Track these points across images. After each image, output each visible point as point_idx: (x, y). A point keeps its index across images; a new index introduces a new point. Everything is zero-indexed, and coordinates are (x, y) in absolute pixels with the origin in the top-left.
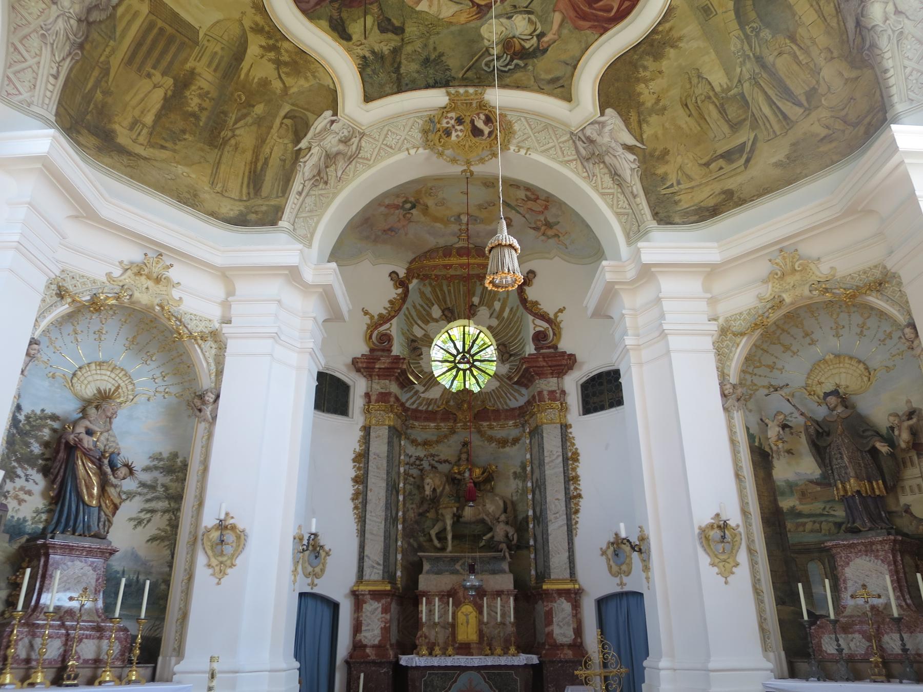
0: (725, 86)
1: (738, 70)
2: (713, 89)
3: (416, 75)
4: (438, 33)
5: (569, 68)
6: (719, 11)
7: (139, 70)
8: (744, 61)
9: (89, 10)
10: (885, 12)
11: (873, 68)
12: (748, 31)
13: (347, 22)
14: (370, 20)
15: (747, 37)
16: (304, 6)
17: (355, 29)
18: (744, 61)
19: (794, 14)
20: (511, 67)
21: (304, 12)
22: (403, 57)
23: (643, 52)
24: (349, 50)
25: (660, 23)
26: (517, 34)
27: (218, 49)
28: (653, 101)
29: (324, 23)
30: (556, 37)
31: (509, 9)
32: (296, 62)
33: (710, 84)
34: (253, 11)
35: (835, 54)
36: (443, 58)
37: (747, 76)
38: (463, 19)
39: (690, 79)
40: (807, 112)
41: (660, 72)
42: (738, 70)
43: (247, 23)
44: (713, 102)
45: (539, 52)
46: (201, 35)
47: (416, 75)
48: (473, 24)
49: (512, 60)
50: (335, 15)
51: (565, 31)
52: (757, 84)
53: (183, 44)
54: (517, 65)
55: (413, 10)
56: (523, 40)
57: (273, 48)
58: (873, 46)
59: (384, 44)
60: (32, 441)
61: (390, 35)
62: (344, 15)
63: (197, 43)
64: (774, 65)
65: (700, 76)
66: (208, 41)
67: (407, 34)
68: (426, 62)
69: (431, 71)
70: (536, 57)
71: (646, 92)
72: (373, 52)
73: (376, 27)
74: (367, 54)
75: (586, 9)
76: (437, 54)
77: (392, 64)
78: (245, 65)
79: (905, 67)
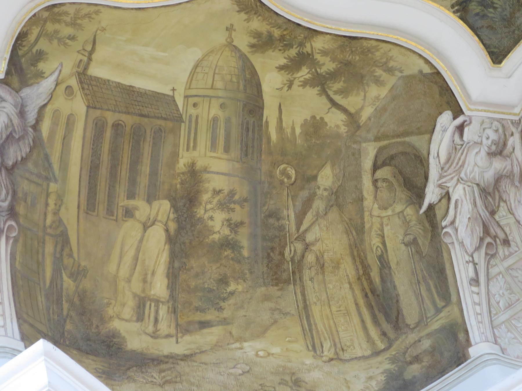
7: (110, 212)
27: (215, 111)
32: (348, 64)
34: (243, 16)
43: (243, 42)
46: (180, 102)
53: (159, 133)
63: (179, 119)
66: (195, 105)
78: (270, 113)
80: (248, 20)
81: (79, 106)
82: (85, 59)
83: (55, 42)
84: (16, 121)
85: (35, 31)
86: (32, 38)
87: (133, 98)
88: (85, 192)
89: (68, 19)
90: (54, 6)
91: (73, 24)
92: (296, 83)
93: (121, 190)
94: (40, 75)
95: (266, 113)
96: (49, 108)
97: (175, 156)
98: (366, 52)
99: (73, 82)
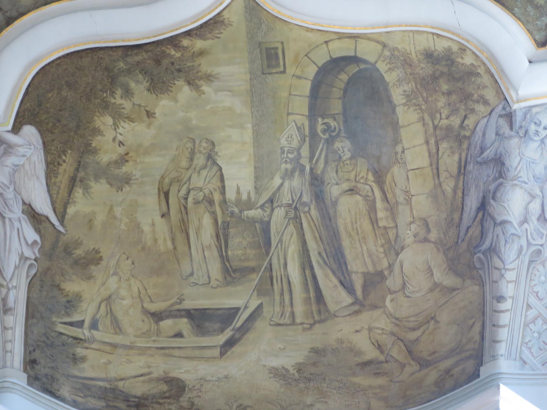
0: (244, 197)
1: (277, 181)
2: (223, 193)
6: (291, 70)
8: (293, 171)
10: (526, 208)
11: (482, 285)
12: (320, 128)
15: (313, 135)
18: (293, 171)
19: (397, 141)
23: (138, 63)
25: (188, 33)
28: (114, 157)
35: (433, 236)
37: (286, 199)
39: (193, 153)
41: (150, 114)
42: (277, 181)
52: (297, 221)
58: (493, 250)
64: (335, 203)
65: (211, 158)
71: (109, 134)
79: (529, 307)
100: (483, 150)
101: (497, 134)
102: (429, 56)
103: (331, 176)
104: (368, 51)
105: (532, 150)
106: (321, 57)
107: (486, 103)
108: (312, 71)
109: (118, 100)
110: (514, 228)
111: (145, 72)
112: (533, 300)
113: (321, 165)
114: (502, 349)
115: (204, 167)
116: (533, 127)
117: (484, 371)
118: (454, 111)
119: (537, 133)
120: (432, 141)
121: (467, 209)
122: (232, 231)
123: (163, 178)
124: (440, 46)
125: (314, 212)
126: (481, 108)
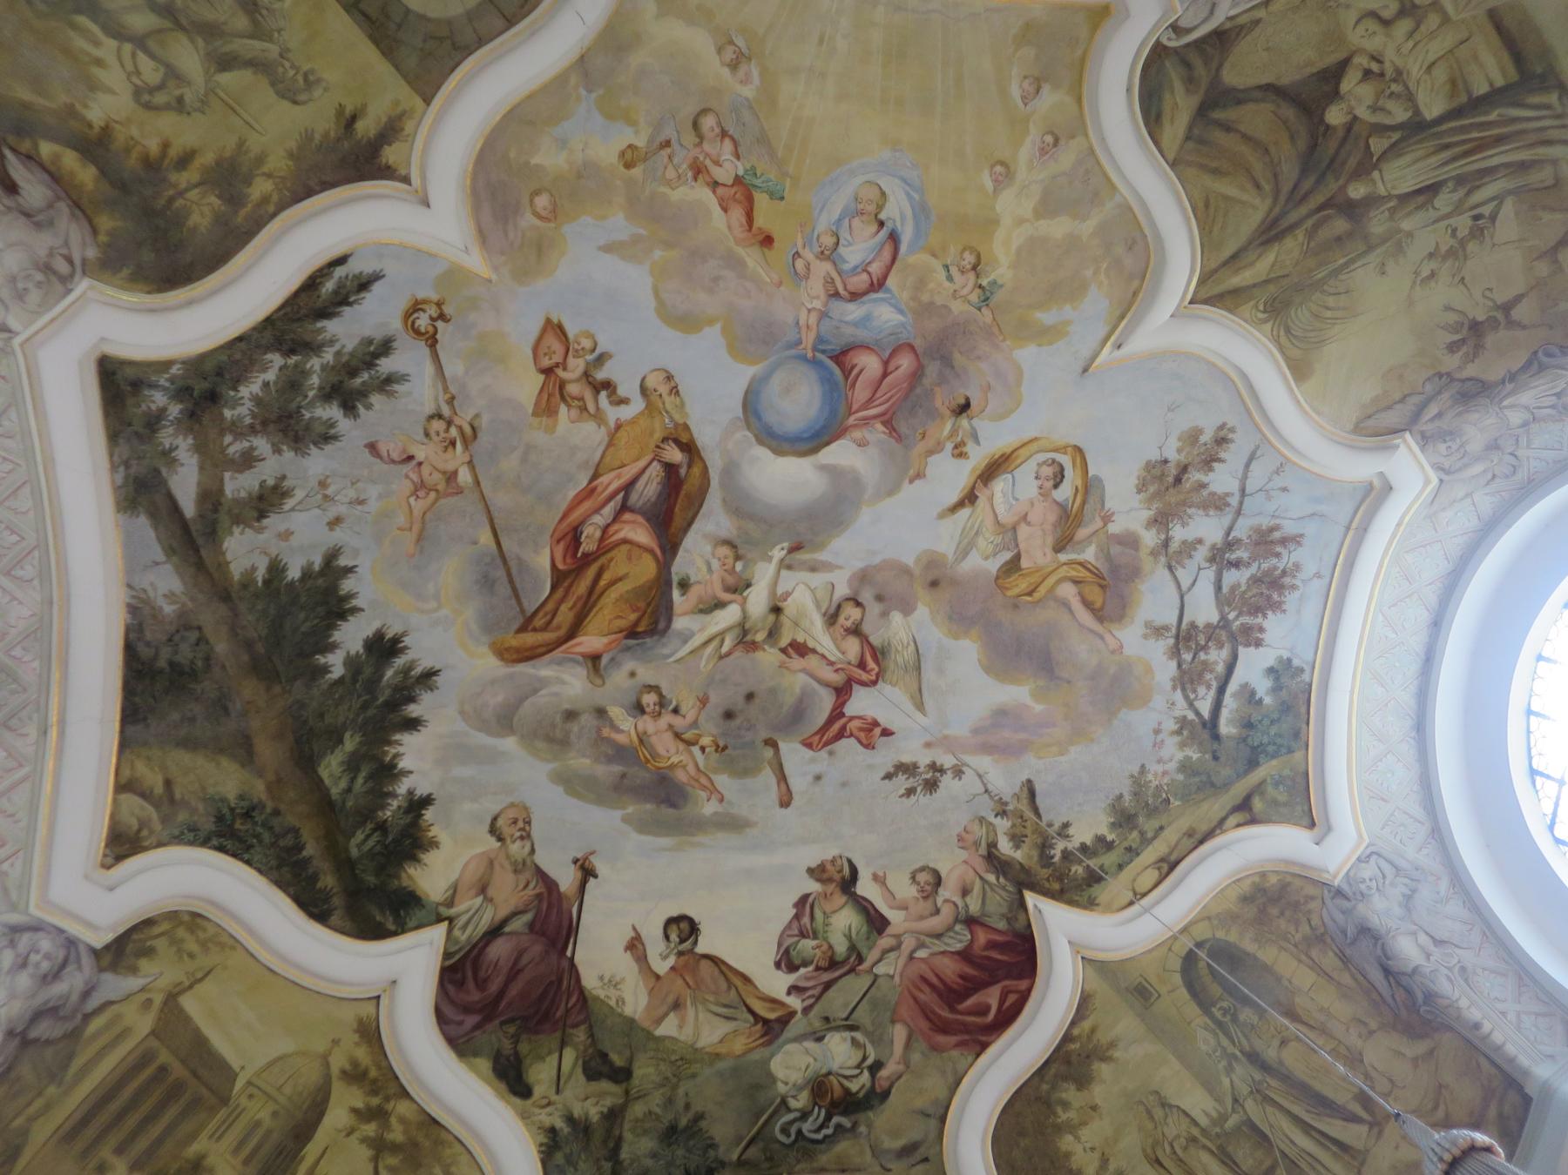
0: (1214, 1114)
1: (1226, 1082)
2: (1196, 1124)
3: (649, 1162)
4: (694, 1076)
5: (933, 1123)
6: (1163, 990)
7: (86, 1153)
8: (1230, 1065)
9: (37, 1016)
10: (1419, 946)
11: (1450, 1028)
12: (1218, 1014)
13: (527, 1061)
14: (569, 1055)
15: (1220, 1024)
16: (453, 1031)
17: (541, 1075)
18: (1230, 1065)
19: (1279, 979)
20: (829, 1131)
21: (451, 1041)
22: (627, 1126)
23: (1056, 1076)
24: (524, 1116)
25: (1073, 1023)
26: (835, 1067)
27: (264, 1115)
28: (1096, 1164)
29: (485, 1064)
30: (901, 1067)
31: (817, 1024)
32: (415, 1145)
33: (1187, 1115)
34: (356, 1037)
35: (1373, 1025)
36: (703, 1124)
37: (1245, 1090)
38: (739, 1046)
39: (1149, 1112)
40: (1376, 1130)
41: (1094, 1108)
42: (1226, 1082)
43: (338, 1062)
44: (1204, 1147)
45: (876, 1097)
46: (239, 1084)
47: (649, 1162)
48: (756, 1056)
49: (828, 1118)
50: (507, 1046)
51: (916, 1057)
52: (1267, 1100)
53: (196, 1103)
54: (839, 1126)
55: (649, 1036)
56: (846, 1077)
57: (377, 1114)
58: (1430, 997)
59: (589, 1101)
60: (1038, 708)
61: (605, 1085)
62: (524, 1048)
63: (224, 1101)
64: (1281, 1063)
65: (1164, 1104)
66: (251, 1096)
67: (635, 1081)
68: (671, 1134)
69: (680, 1152)
70: (871, 1108)
71: (1078, 1149)
72: (570, 1119)
73: (579, 1070)
74: (559, 1124)
75: (946, 1014)
76: (690, 1115)
77: (605, 1142)
78: (311, 1151)
79: (1503, 1014)
80: (357, 1044)
81: (143, 1024)
82: (187, 984)
83: (174, 949)
84: (75, 998)
85: (165, 926)
86: (156, 930)
87: (199, 1051)
88: (78, 1116)
89: (201, 935)
90: (199, 915)
91: (204, 945)
92: (357, 1135)
93: (113, 1140)
94: (134, 970)
95: (309, 1146)
96: (115, 1007)
97: (193, 1136)
98: (439, 1143)
99: (158, 999)
100: (1344, 933)
101: (1343, 913)
102: (1246, 899)
103: (1259, 1045)
104: (1202, 932)
105: (1378, 903)
106: (1176, 964)
107: (1313, 898)
108: (1177, 979)
109: (1063, 1116)
110: (1427, 967)
111: (1065, 1078)
112: (1500, 1006)
113: (1244, 1042)
114: (1524, 1061)
115: (1166, 1116)
116: (1363, 887)
117: (1530, 1090)
118: (1297, 924)
119: (1369, 888)
120: (1303, 957)
121: (1378, 985)
122: (1230, 1149)
123: (1144, 1151)
124: (1246, 886)
125: (1274, 1083)
126: (1313, 905)
